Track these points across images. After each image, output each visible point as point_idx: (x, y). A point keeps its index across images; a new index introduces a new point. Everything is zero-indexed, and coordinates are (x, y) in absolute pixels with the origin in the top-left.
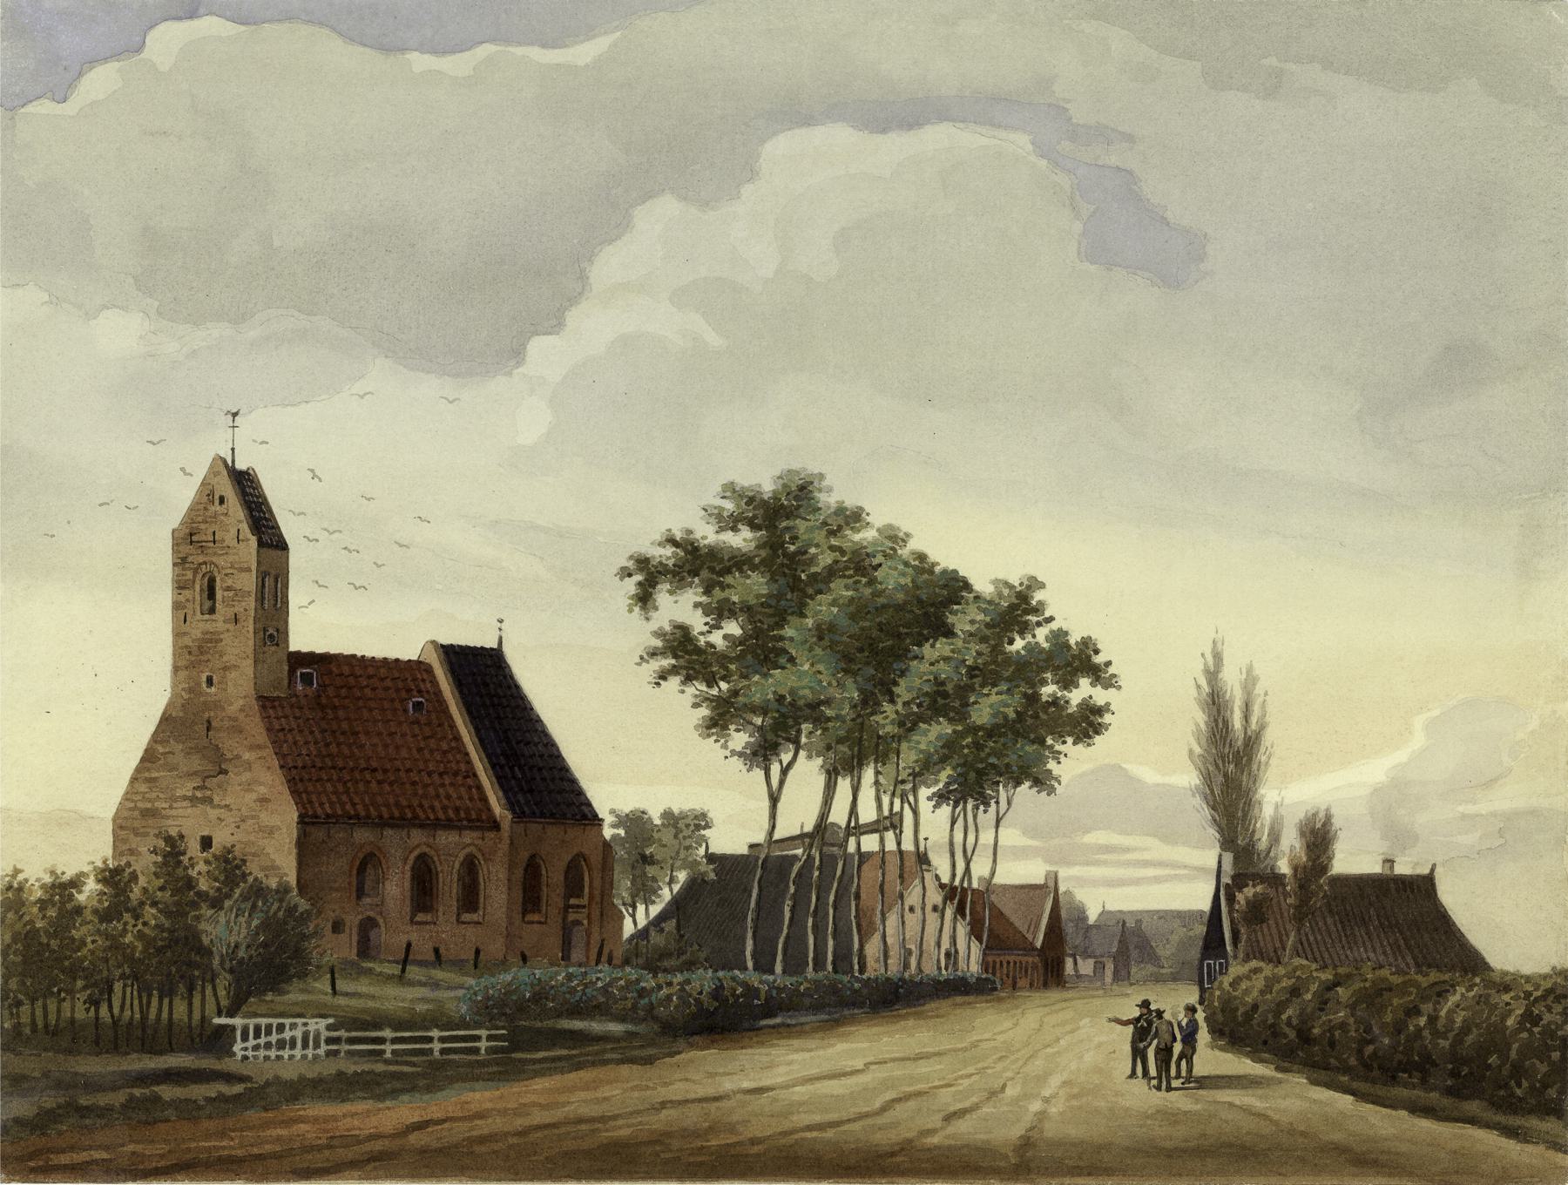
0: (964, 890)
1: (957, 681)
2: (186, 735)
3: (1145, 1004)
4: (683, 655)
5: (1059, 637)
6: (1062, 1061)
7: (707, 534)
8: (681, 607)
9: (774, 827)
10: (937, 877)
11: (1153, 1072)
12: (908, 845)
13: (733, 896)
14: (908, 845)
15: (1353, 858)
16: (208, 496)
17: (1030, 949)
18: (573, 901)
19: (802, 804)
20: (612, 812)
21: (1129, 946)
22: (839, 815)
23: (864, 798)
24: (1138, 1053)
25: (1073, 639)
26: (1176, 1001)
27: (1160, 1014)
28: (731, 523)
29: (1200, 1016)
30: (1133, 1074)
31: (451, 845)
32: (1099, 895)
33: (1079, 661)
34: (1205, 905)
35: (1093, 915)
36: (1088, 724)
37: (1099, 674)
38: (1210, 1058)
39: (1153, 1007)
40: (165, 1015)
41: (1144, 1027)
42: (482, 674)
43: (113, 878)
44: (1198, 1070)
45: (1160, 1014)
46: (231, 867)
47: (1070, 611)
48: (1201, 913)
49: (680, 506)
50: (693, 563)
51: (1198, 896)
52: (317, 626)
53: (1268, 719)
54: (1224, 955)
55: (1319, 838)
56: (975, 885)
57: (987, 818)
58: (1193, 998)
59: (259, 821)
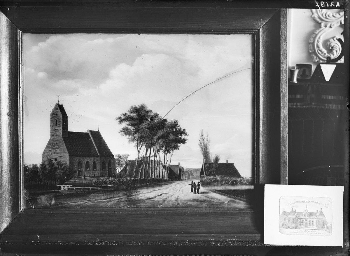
0: (166, 166)
1: (168, 135)
2: (52, 145)
3: (192, 182)
4: (126, 131)
5: (180, 129)
6: (180, 192)
7: (129, 114)
8: (125, 124)
9: (139, 156)
10: (162, 163)
11: (194, 191)
12: (158, 159)
13: (134, 166)
14: (158, 159)
15: (222, 161)
16: (55, 109)
17: (175, 174)
18: (110, 168)
19: (143, 153)
20: (116, 156)
21: (190, 172)
22: (148, 155)
23: (152, 152)
24: (192, 189)
25: (182, 129)
26: (196, 182)
27: (195, 183)
28: (133, 112)
29: (200, 183)
30: (191, 192)
31: (91, 160)
32: (186, 166)
33: (183, 132)
34: (201, 168)
35: (185, 169)
36: (183, 141)
37: (186, 134)
38: (202, 189)
39: (194, 182)
40: (150, 159)
41: (193, 185)
42: (96, 135)
43: (43, 165)
44: (200, 191)
45: (195, 183)
46: (59, 164)
47: (182, 125)
48: (199, 169)
49: (125, 109)
50: (127, 118)
51: (199, 166)
52: (71, 128)
53: (121, 130)
54: (203, 174)
55: (217, 159)
56: (168, 165)
57: (169, 154)
58: (199, 181)
59: (65, 158)
